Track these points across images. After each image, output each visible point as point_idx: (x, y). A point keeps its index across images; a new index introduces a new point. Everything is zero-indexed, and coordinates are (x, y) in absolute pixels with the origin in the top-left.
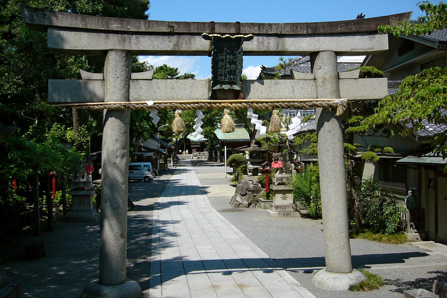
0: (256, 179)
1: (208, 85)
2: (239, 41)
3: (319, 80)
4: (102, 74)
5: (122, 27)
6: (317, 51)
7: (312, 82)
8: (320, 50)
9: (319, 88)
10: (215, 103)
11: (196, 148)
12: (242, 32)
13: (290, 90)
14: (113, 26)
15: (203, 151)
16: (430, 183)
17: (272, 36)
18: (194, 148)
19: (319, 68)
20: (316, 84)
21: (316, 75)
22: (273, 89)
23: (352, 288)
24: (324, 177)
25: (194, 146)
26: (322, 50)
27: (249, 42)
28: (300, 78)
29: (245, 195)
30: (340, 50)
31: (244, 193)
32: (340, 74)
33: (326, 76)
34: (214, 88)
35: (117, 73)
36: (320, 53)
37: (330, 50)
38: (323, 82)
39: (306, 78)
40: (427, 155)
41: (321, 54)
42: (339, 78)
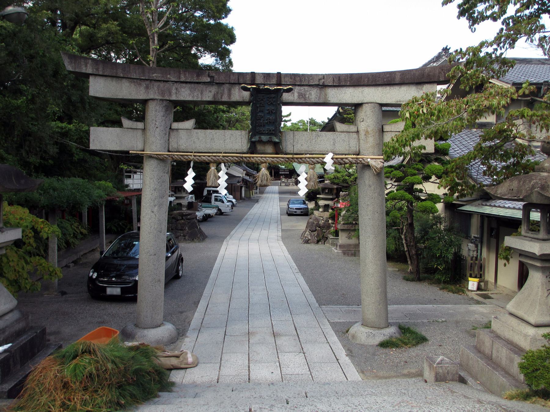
0: (327, 215)
1: (247, 136)
2: (278, 92)
3: (362, 133)
4: (143, 123)
5: (163, 77)
6: (360, 102)
7: (355, 135)
8: (363, 102)
9: (361, 141)
10: (253, 157)
11: (284, 174)
12: (283, 83)
13: (332, 143)
14: (154, 75)
15: (291, 178)
16: (492, 232)
17: (314, 87)
18: (282, 175)
19: (361, 120)
20: (359, 137)
21: (359, 127)
22: (314, 141)
23: (384, 345)
24: (363, 231)
25: (283, 173)
26: (365, 101)
27: (290, 94)
28: (342, 130)
29: (315, 231)
30: (384, 101)
31: (314, 228)
32: (384, 127)
33: (369, 130)
34: (253, 140)
35: (157, 123)
36: (364, 105)
37: (374, 101)
38: (365, 135)
39: (349, 130)
40: (488, 204)
41: (364, 106)
42: (383, 131)
